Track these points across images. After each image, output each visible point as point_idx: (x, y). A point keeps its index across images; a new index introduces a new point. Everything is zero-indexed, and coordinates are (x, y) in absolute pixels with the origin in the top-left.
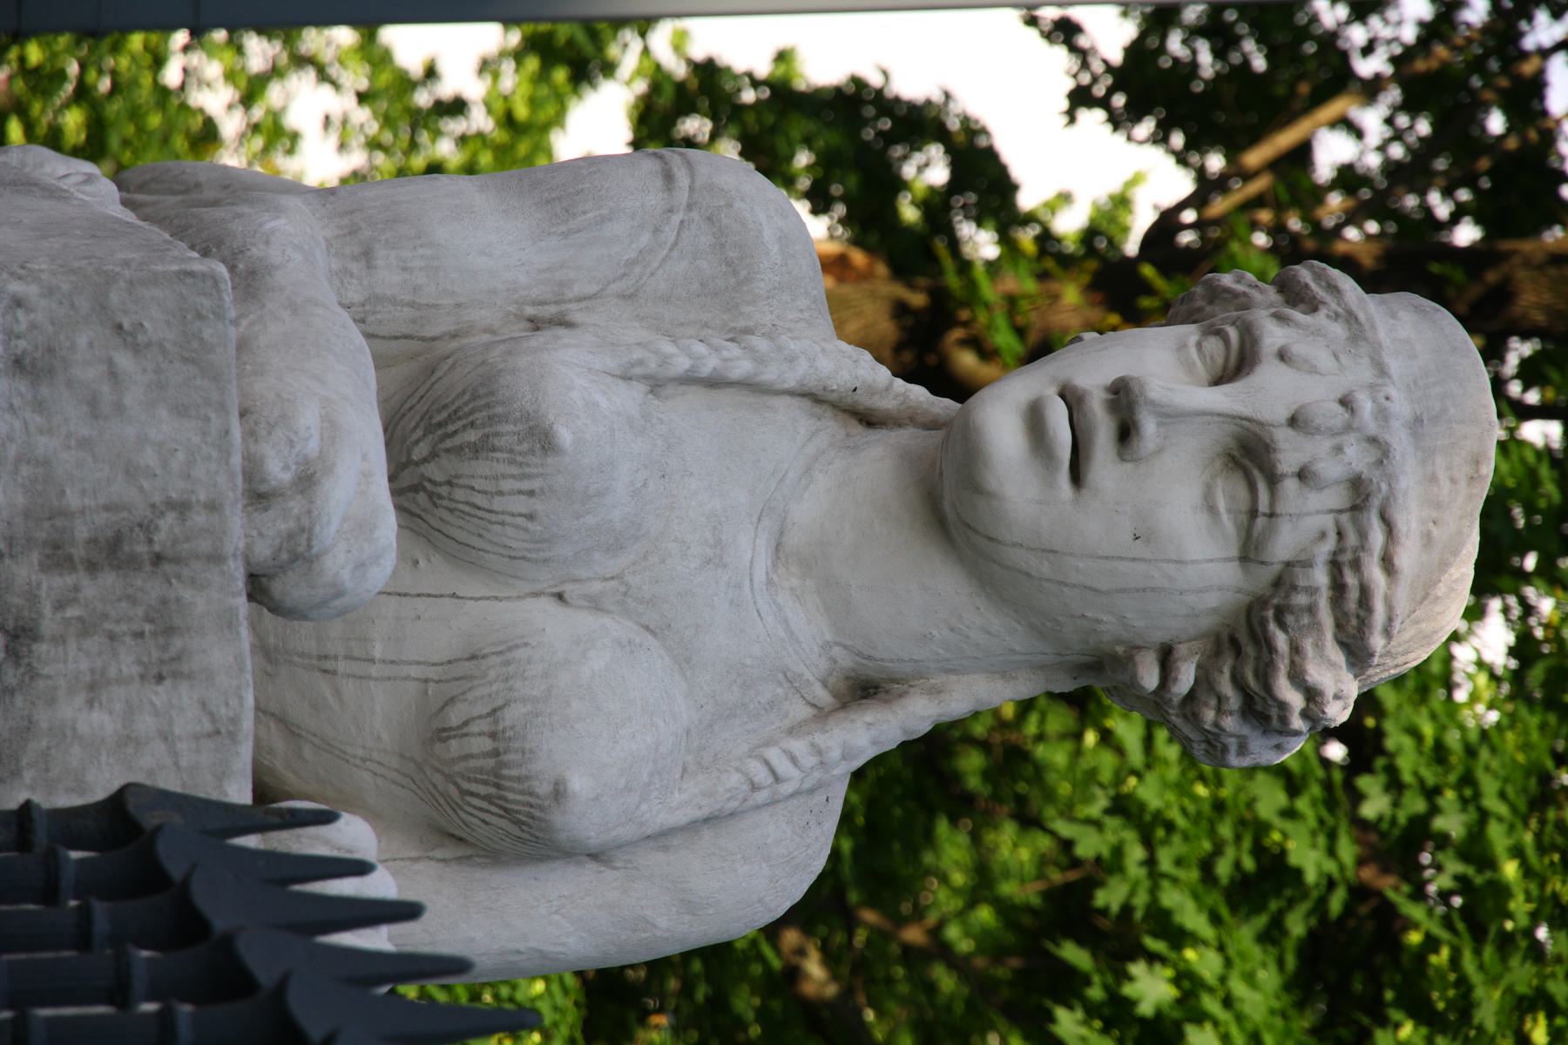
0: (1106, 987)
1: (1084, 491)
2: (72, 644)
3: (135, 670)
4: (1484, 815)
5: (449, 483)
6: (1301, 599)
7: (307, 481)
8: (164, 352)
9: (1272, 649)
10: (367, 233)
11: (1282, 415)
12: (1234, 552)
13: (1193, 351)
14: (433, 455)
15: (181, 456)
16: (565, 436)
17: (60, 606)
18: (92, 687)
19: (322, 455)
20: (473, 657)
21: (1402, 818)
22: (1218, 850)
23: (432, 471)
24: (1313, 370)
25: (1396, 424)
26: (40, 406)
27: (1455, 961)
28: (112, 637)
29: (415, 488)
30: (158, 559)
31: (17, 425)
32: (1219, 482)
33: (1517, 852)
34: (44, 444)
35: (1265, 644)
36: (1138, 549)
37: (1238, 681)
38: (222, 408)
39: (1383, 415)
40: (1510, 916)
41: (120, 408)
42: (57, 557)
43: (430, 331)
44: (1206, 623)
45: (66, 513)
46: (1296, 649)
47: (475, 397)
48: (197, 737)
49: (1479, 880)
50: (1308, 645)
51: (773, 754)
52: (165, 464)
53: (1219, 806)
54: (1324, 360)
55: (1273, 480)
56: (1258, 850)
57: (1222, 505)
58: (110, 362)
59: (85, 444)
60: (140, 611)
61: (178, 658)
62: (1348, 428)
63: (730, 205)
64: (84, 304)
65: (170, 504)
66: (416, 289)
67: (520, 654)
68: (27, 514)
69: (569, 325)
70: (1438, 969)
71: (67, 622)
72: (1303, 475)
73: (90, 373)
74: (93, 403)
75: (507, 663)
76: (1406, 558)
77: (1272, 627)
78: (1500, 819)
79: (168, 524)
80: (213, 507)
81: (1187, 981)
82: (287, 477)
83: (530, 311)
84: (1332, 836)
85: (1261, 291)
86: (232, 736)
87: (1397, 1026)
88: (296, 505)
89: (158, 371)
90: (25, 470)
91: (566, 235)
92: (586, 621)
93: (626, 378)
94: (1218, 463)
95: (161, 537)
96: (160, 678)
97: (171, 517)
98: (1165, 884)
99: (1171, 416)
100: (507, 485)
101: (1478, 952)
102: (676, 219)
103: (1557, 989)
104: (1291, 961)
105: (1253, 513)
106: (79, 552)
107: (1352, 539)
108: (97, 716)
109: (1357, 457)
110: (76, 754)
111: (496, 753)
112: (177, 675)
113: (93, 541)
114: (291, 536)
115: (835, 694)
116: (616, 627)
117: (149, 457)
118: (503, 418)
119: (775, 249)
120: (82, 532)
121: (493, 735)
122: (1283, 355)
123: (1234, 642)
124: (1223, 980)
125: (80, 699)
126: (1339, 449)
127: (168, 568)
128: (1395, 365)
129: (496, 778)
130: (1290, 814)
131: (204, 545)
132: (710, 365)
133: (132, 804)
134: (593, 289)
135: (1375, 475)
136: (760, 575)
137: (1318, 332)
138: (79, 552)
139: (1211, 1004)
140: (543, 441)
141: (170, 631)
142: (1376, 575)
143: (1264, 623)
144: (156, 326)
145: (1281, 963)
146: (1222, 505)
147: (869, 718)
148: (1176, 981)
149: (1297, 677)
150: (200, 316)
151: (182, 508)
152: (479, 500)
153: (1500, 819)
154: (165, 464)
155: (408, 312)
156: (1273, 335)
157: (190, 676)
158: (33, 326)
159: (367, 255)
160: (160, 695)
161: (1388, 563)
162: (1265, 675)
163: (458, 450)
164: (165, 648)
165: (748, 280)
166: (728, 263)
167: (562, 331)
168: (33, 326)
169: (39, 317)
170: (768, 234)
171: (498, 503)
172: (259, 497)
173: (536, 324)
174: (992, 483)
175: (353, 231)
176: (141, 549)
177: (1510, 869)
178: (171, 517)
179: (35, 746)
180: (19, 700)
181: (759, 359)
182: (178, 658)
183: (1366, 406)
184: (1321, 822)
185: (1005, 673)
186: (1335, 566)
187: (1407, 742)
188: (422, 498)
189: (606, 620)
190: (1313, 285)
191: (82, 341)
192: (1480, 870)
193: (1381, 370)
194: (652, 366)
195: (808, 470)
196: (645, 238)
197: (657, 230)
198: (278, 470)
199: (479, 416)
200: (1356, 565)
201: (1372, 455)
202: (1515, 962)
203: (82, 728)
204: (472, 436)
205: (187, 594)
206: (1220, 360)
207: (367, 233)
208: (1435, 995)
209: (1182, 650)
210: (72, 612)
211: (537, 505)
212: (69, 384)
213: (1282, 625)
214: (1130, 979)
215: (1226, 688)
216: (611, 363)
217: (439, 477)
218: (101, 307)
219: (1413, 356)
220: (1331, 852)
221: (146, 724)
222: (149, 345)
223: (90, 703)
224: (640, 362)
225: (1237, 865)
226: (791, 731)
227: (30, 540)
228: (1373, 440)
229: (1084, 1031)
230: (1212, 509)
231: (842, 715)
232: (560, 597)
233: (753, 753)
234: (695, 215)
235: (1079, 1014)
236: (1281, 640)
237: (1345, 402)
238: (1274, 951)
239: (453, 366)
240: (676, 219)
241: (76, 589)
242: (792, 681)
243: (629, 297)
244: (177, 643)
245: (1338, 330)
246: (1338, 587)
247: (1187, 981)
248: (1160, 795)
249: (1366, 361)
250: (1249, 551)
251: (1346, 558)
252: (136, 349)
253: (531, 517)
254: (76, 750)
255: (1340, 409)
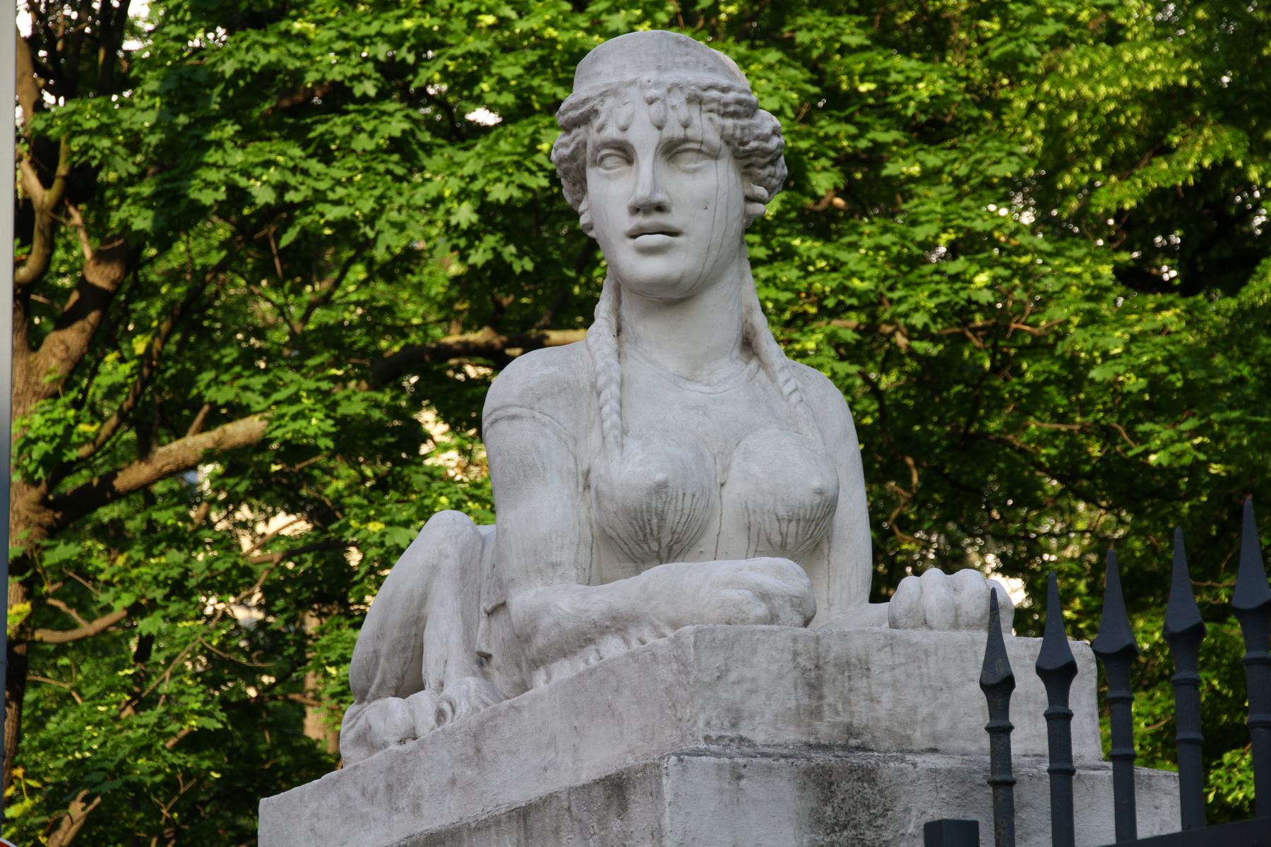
0: (459, 237)
1: (684, 230)
2: (854, 708)
3: (865, 680)
4: (379, 34)
5: (673, 533)
6: (738, 133)
7: (765, 596)
8: (729, 658)
9: (756, 149)
10: (542, 565)
11: (656, 132)
12: (712, 162)
13: (610, 172)
14: (659, 541)
15: (774, 653)
16: (660, 477)
17: (837, 713)
18: (872, 700)
19: (750, 589)
20: (749, 528)
21: (377, 75)
22: (388, 172)
23: (665, 542)
24: (632, 116)
25: (661, 79)
26: (752, 717)
27: (453, 58)
28: (851, 690)
29: (670, 549)
30: (817, 667)
31: (760, 727)
32: (682, 166)
33: (399, 20)
34: (768, 716)
35: (750, 154)
36: (711, 208)
37: (763, 167)
38: (753, 632)
39: (657, 85)
40: (431, 27)
41: (753, 680)
42: (816, 713)
43: (590, 539)
44: (739, 180)
45: (798, 708)
46: (757, 138)
47: (636, 519)
48: (893, 654)
49: (413, 41)
50: (757, 132)
51: (787, 390)
52: (777, 661)
53: (366, 170)
54: (627, 110)
55: (686, 140)
56: (389, 151)
57: (693, 166)
58: (734, 683)
59: (768, 697)
60: (840, 677)
61: (859, 660)
62: (664, 102)
63: (531, 389)
64: (708, 694)
65: (794, 659)
66: (572, 543)
67: (751, 506)
68: (798, 726)
69: (589, 471)
70: (457, 67)
71: (844, 710)
72: (686, 126)
73: (738, 692)
74: (752, 692)
75: (755, 512)
76: (724, 82)
77: (747, 148)
78: (382, 26)
79: (803, 661)
80: (795, 640)
81: (462, 196)
82: (764, 605)
83: (581, 489)
84: (383, 113)
85: (577, 135)
86: (892, 638)
87: (482, 91)
88: (777, 602)
89: (737, 661)
90: (779, 725)
91: (545, 469)
92: (734, 474)
93: (622, 446)
94: (672, 165)
95: (808, 665)
96: (868, 669)
97: (799, 660)
98: (412, 202)
99: (655, 187)
100: (679, 506)
101: (451, 46)
102: (538, 415)
103: (467, 7)
104: (440, 141)
105: (699, 151)
106: (814, 703)
107: (714, 106)
108: (884, 699)
109: (678, 99)
110: (901, 710)
111: (798, 521)
112: (867, 662)
113: (810, 696)
114: (793, 606)
115: (750, 358)
116: (737, 459)
117: (774, 668)
118: (649, 505)
119: (552, 369)
120: (806, 701)
121: (790, 521)
122: (624, 129)
123: (747, 167)
124: (462, 178)
125: (877, 706)
126: (674, 107)
127: (821, 662)
128: (629, 76)
129: (809, 521)
130: (372, 134)
131: (812, 645)
132: (614, 404)
133: (992, 681)
134: (571, 458)
135: (687, 91)
136: (707, 389)
137: (611, 111)
138: (814, 703)
139: (476, 186)
140: (661, 487)
141: (848, 663)
142: (731, 96)
143: (745, 151)
144: (718, 660)
145: (441, 146)
146: (693, 166)
147: (765, 343)
148: (460, 202)
149: (766, 138)
150: (713, 640)
151: (796, 654)
152: (684, 520)
153: (382, 26)
154: (777, 661)
155: (582, 545)
156: (612, 133)
157: (867, 655)
158: (718, 718)
159: (554, 565)
160: (875, 669)
161: (725, 90)
162: (765, 153)
163: (660, 528)
164: (856, 666)
165: (568, 383)
166: (560, 392)
167: (593, 475)
168: (718, 718)
169: (714, 714)
170: (546, 371)
171: (686, 511)
172: (773, 618)
173: (587, 487)
174: (677, 275)
175: (540, 571)
176: (813, 674)
177: (408, 24)
178: (799, 660)
179: (897, 729)
180: (877, 734)
181: (610, 381)
182: (859, 660)
183: (652, 92)
184: (375, 118)
185: (742, 277)
186: (725, 115)
187: (337, 69)
188: (675, 547)
189: (734, 464)
190: (581, 111)
191: (725, 695)
192: (408, 39)
193: (633, 83)
194: (617, 432)
195: (652, 362)
196: (548, 431)
197: (544, 425)
198: (761, 610)
199: (646, 516)
200: (726, 105)
201: (677, 92)
202: (452, 27)
203: (889, 706)
204: (655, 521)
205: (832, 655)
206: (618, 159)
207: (542, 565)
208: (470, 70)
209: (748, 192)
210: (840, 708)
211: (689, 493)
212: (743, 703)
213: (747, 143)
214: (458, 225)
215: (765, 172)
216: (617, 452)
217: (669, 539)
218: (710, 685)
219: (624, 67)
220: (391, 114)
221: (887, 677)
222: (726, 665)
223: (879, 702)
224: (616, 438)
225: (396, 163)
226: (773, 380)
227: (809, 725)
228: (669, 90)
229: (481, 250)
230: (695, 171)
231: (762, 356)
232: (722, 485)
233: (787, 400)
234: (536, 406)
235: (472, 251)
236: (753, 144)
237: (651, 102)
238: (436, 150)
239: (612, 528)
240: (538, 415)
241: (830, 705)
242: (751, 379)
243: (576, 440)
244: (853, 660)
245: (610, 101)
246: (734, 115)
247: (462, 196)
248: (367, 200)
249: (628, 90)
250: (714, 155)
251: (722, 109)
252: (728, 670)
253: (694, 496)
254: (899, 709)
255: (654, 106)
